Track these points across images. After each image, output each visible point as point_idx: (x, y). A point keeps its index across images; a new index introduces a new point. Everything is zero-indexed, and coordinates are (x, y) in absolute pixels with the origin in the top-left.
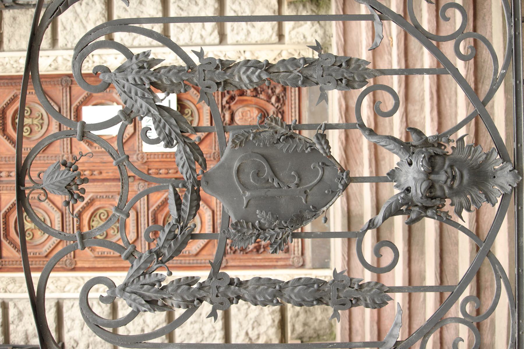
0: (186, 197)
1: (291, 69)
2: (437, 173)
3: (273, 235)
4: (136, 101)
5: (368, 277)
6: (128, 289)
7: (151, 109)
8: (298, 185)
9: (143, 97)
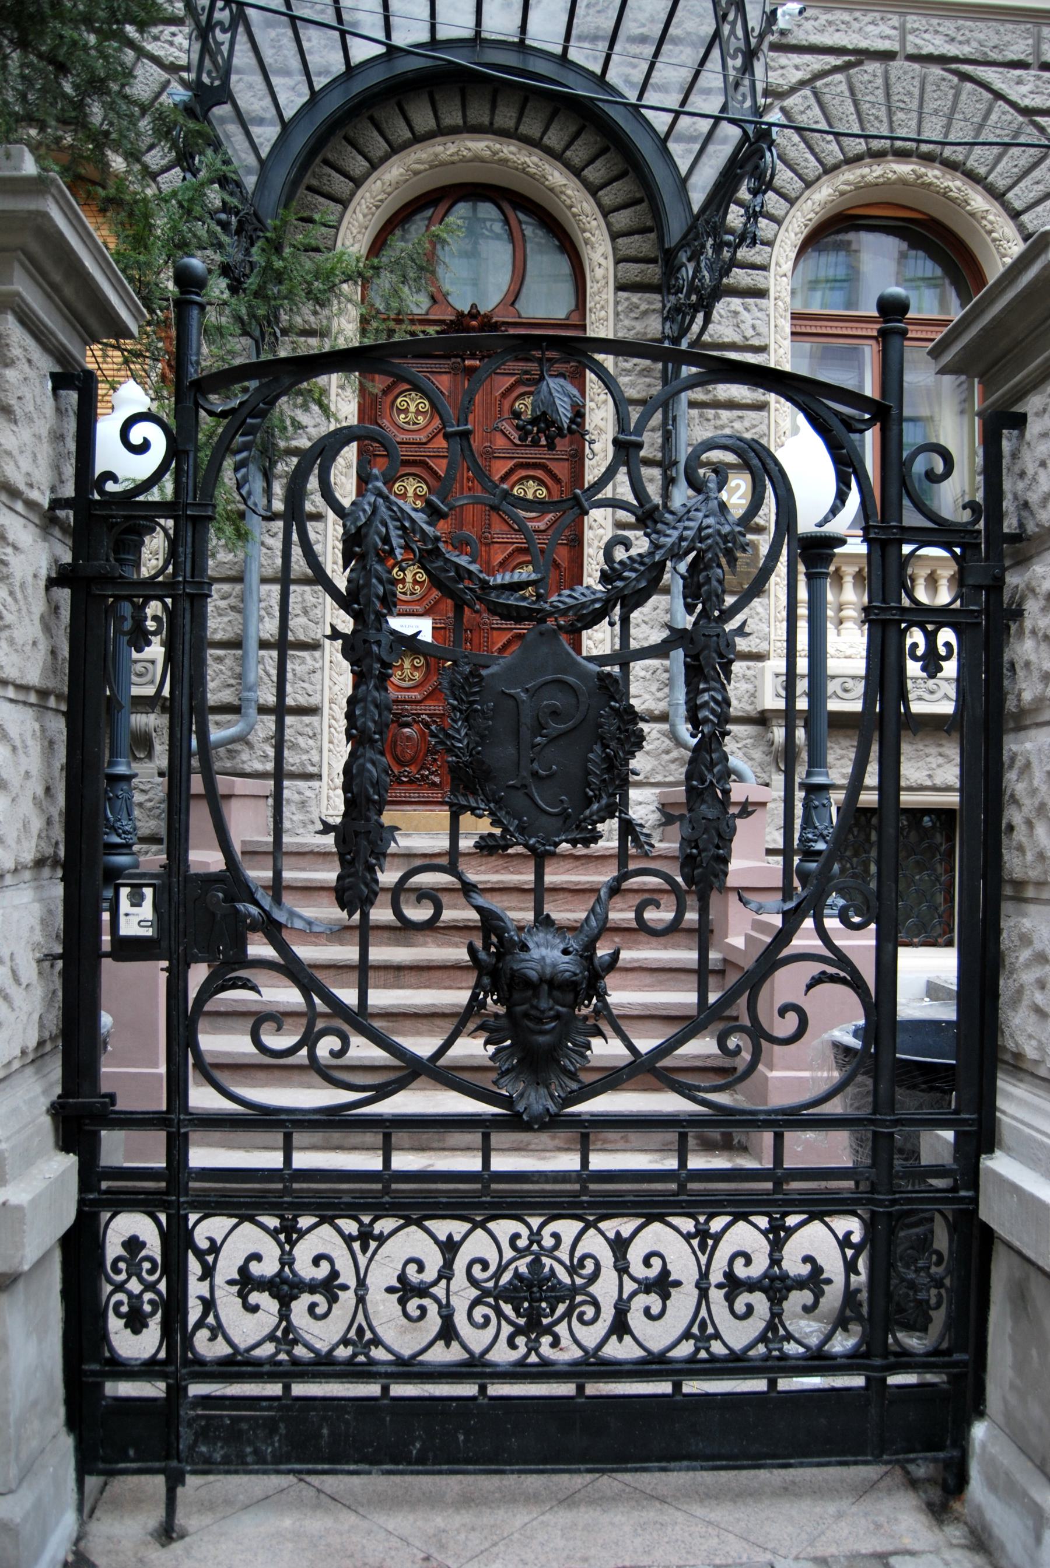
0: (524, 598)
1: (715, 770)
2: (550, 995)
3: (459, 733)
4: (675, 528)
5: (388, 877)
6: (380, 501)
7: (662, 551)
8: (535, 774)
9: (681, 538)
